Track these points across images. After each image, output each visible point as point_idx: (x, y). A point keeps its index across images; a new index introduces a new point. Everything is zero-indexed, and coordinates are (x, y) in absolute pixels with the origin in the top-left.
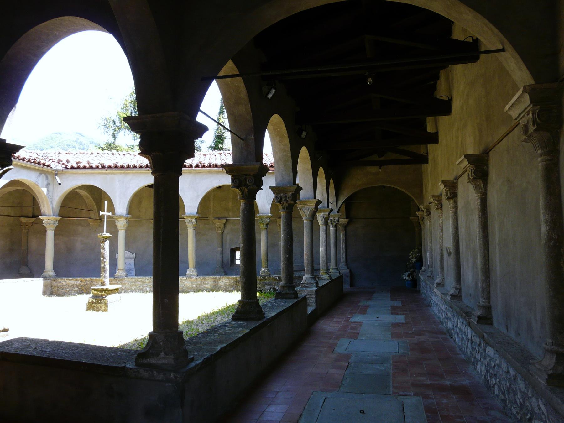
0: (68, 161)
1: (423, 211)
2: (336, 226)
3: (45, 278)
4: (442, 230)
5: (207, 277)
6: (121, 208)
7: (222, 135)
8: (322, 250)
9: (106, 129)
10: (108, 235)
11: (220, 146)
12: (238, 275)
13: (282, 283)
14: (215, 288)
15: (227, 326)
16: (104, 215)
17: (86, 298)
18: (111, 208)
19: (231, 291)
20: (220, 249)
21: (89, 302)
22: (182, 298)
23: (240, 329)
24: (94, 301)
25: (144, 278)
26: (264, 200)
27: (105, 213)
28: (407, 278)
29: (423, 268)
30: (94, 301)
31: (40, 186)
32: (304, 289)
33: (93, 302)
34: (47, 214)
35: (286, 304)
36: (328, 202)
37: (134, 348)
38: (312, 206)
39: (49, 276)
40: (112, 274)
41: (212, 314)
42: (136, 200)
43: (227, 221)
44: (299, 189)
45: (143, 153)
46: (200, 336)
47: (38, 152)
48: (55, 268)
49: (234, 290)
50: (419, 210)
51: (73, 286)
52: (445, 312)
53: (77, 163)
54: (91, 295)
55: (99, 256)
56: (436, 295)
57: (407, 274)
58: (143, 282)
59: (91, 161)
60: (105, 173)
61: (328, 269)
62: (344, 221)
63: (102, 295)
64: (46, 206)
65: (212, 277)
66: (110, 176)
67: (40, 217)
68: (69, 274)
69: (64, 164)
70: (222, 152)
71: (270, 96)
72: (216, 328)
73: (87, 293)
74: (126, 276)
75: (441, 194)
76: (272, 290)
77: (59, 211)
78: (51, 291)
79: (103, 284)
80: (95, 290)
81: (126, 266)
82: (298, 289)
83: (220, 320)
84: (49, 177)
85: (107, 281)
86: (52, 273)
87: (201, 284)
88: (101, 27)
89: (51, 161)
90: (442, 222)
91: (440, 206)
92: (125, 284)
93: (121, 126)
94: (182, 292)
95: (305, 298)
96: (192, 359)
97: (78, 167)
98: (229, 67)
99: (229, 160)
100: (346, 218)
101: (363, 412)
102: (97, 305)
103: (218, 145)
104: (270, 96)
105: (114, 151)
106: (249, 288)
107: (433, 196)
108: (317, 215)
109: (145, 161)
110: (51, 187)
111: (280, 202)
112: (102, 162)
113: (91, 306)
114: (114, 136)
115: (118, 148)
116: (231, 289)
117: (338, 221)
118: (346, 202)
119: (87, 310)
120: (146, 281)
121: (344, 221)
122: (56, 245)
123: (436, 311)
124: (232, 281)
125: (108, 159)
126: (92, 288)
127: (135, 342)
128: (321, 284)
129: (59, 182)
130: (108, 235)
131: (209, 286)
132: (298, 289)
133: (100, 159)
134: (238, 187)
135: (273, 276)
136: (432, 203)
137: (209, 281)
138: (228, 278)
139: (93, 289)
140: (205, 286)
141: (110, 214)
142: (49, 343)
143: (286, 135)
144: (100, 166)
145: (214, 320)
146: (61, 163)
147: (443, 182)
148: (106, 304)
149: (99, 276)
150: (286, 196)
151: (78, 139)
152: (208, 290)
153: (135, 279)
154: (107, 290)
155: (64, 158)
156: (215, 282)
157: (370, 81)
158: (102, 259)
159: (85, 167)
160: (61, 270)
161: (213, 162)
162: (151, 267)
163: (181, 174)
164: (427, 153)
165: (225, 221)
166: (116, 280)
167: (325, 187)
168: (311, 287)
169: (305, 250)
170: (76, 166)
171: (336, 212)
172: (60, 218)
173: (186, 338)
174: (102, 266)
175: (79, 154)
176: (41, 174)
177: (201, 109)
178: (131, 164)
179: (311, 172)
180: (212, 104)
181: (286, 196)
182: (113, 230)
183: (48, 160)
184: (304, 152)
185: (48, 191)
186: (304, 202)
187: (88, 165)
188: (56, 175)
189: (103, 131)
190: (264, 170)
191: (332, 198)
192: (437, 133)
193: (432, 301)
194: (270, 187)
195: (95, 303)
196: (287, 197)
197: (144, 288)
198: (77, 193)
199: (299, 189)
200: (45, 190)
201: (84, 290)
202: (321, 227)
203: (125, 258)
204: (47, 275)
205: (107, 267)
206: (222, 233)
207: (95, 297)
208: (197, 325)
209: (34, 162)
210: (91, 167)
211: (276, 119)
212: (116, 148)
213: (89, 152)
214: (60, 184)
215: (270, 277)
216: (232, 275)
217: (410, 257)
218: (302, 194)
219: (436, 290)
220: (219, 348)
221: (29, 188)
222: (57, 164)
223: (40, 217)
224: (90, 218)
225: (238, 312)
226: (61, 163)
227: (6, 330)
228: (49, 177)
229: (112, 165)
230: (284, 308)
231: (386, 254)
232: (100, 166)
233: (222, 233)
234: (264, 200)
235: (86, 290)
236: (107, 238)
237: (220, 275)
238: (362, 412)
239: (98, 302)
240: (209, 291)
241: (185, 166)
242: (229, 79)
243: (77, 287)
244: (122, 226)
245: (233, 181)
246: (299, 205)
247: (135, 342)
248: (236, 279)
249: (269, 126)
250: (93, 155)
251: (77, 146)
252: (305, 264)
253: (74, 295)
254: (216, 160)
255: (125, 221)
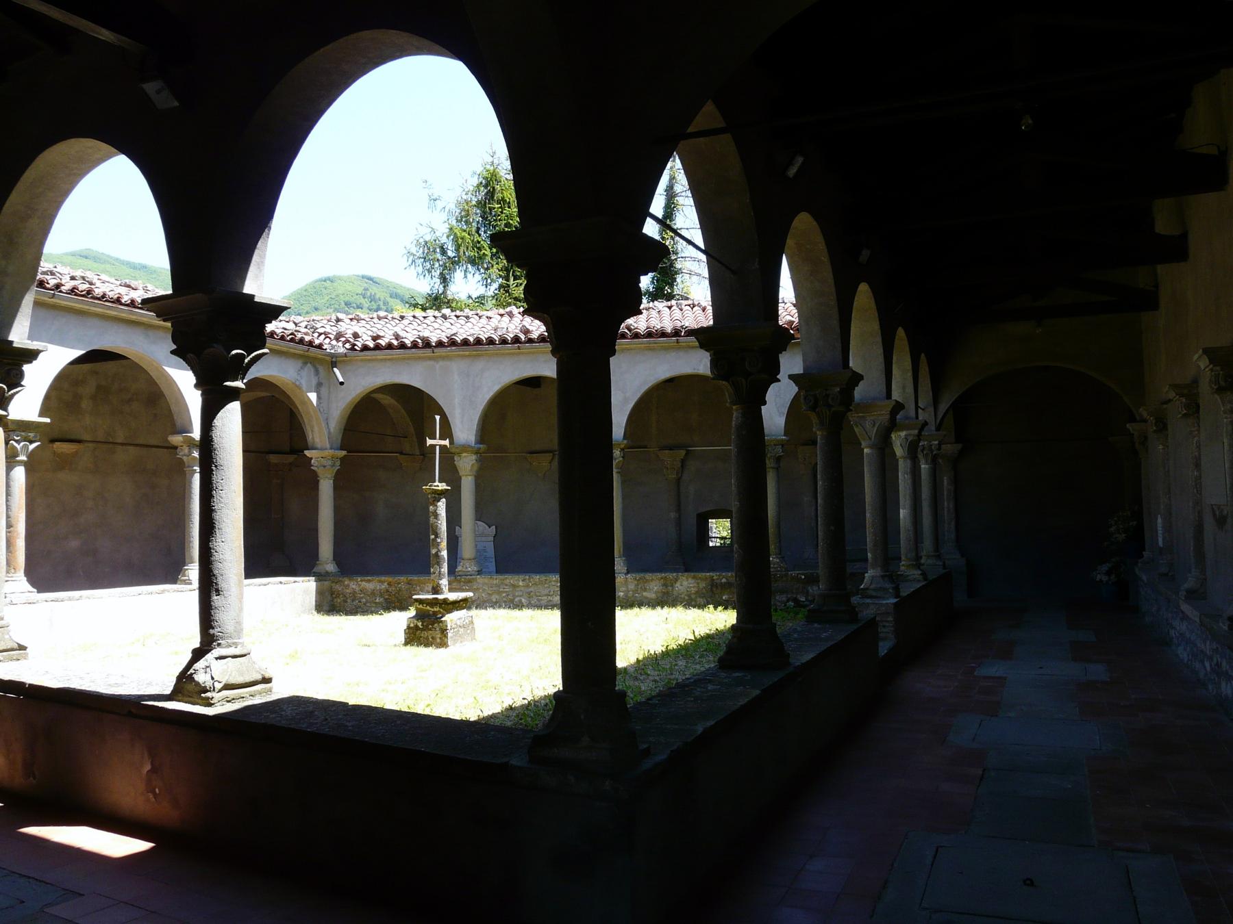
0: (356, 336)
1: (1145, 421)
2: (934, 461)
3: (320, 577)
4: (1198, 465)
5: (648, 576)
6: (465, 430)
8: (903, 513)
9: (428, 265)
10: (442, 486)
11: (667, 290)
14: (665, 600)
15: (710, 681)
16: (434, 446)
17: (400, 620)
18: (447, 432)
19: (701, 607)
20: (673, 515)
21: (409, 627)
22: (623, 618)
23: (740, 689)
24: (420, 624)
25: (516, 577)
28: (1105, 578)
29: (1146, 554)
30: (420, 624)
32: (868, 601)
34: (319, 446)
35: (831, 635)
36: (917, 407)
37: (509, 724)
38: (882, 416)
40: (452, 571)
41: (666, 654)
43: (688, 452)
44: (857, 378)
45: (532, 311)
46: (655, 701)
48: (338, 557)
49: (709, 603)
50: (1133, 419)
51: (373, 593)
52: (1211, 658)
53: (375, 338)
54: (412, 612)
55: (426, 530)
56: (1185, 617)
57: (1105, 568)
58: (514, 586)
59: (402, 334)
60: (430, 358)
61: (918, 558)
62: (951, 448)
63: (435, 613)
64: (316, 429)
65: (659, 575)
66: (441, 363)
67: (306, 452)
68: (364, 570)
70: (673, 302)
71: (792, 172)
72: (687, 686)
73: (403, 608)
74: (480, 572)
75: (1195, 382)
76: (791, 603)
78: (329, 604)
79: (436, 590)
80: (420, 601)
81: (478, 551)
83: (685, 671)
84: (321, 369)
85: (444, 582)
86: (331, 567)
87: (635, 591)
90: (1199, 447)
91: (1193, 409)
93: (459, 257)
94: (629, 604)
95: (872, 623)
96: (647, 753)
99: (707, 320)
100: (957, 442)
101: (1032, 884)
104: (792, 172)
105: (446, 311)
106: (752, 600)
107: (1174, 387)
108: (893, 436)
109: (537, 328)
110: (324, 390)
111: (813, 408)
112: (426, 334)
113: (414, 636)
114: (444, 280)
115: (454, 305)
116: (701, 601)
117: (939, 449)
118: (954, 406)
119: (406, 644)
121: (951, 448)
122: (337, 509)
123: (1183, 653)
124: (702, 585)
125: (436, 328)
127: (511, 713)
128: (906, 591)
129: (341, 380)
130: (442, 486)
131: (653, 596)
132: (855, 600)
133: (419, 328)
134: (726, 379)
135: (794, 573)
136: (1170, 401)
138: (694, 578)
139: (416, 600)
141: (446, 442)
143: (825, 259)
144: (420, 345)
147: (1206, 351)
148: (444, 631)
149: (429, 573)
150: (827, 396)
151: (366, 289)
152: (654, 604)
153: (497, 579)
154: (445, 601)
155: (348, 328)
156: (665, 585)
157: (1026, 123)
159: (390, 346)
160: (353, 561)
162: (555, 553)
163: (613, 352)
164: (1157, 286)
165: (683, 452)
166: (459, 581)
167: (910, 374)
168: (884, 598)
169: (868, 515)
170: (371, 344)
171: (933, 428)
172: (344, 453)
173: (630, 704)
174: (434, 551)
175: (376, 320)
176: (305, 363)
178: (483, 337)
179: (879, 339)
181: (827, 396)
184: (864, 295)
185: (319, 398)
186: (866, 407)
187: (395, 343)
188: (334, 364)
189: (420, 269)
190: (783, 338)
191: (925, 399)
192: (1184, 236)
193: (1172, 632)
195: (422, 630)
196: (826, 395)
198: (375, 401)
199: (857, 378)
200: (313, 396)
201: (394, 603)
202: (901, 463)
203: (476, 536)
205: (444, 553)
206: (678, 480)
207: (420, 616)
208: (636, 679)
209: (292, 340)
210: (402, 346)
211: (803, 222)
212: (448, 303)
213: (396, 315)
214: (342, 383)
215: (786, 575)
216: (702, 570)
217: (1112, 529)
218: (859, 392)
219: (1185, 607)
220: (700, 729)
222: (334, 342)
223: (306, 452)
224: (401, 453)
225: (730, 649)
227: (266, 680)
228: (321, 369)
229: (445, 340)
231: (1057, 519)
232: (420, 345)
233: (678, 480)
235: (400, 601)
236: (442, 493)
238: (1029, 882)
239: (427, 630)
240: (654, 607)
241: (624, 336)
242: (702, 139)
243: (381, 596)
244: (469, 468)
245: (714, 364)
246: (852, 417)
247: (511, 713)
249: (790, 242)
250: (405, 322)
252: (869, 545)
253: (376, 613)
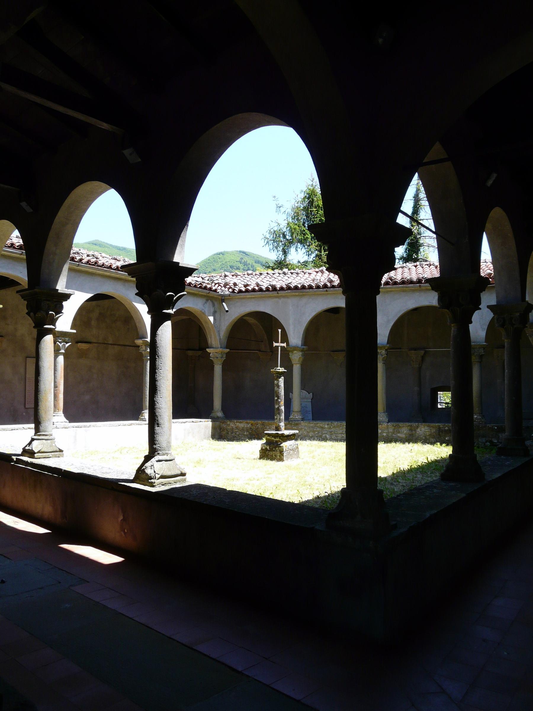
0: (235, 284)
3: (214, 420)
5: (401, 424)
6: (296, 338)
7: (417, 241)
9: (276, 244)
10: (282, 370)
12: (448, 422)
13: (503, 436)
14: (411, 439)
17: (257, 445)
18: (285, 338)
19: (433, 443)
20: (416, 389)
21: (262, 449)
22: (382, 447)
24: (268, 447)
25: (324, 423)
26: (479, 326)
27: (279, 344)
30: (268, 447)
31: (207, 314)
33: (266, 448)
34: (214, 346)
39: (218, 417)
40: (287, 418)
42: (316, 327)
43: (426, 352)
47: (204, 276)
48: (224, 409)
51: (243, 429)
53: (246, 286)
54: (264, 441)
55: (273, 394)
58: (322, 428)
59: (261, 283)
65: (408, 424)
66: (282, 299)
67: (207, 350)
69: (231, 288)
70: (418, 263)
71: (490, 183)
74: (303, 419)
76: (488, 444)
77: (227, 343)
78: (220, 434)
79: (278, 428)
80: (269, 435)
81: (302, 407)
82: (528, 443)
85: (282, 424)
86: (220, 414)
87: (393, 433)
88: (279, 120)
89: (217, 285)
92: (302, 429)
93: (293, 239)
97: (247, 291)
98: (437, 151)
99: (434, 272)
102: (271, 453)
103: (412, 256)
104: (490, 183)
105: (286, 270)
110: (217, 315)
111: (503, 326)
112: (274, 283)
113: (265, 454)
114: (285, 253)
116: (432, 440)
119: (260, 458)
120: (326, 426)
122: (224, 382)
124: (433, 430)
125: (280, 280)
126: (266, 432)
127: (318, 500)
129: (227, 309)
130: (282, 370)
132: (528, 443)
133: (270, 280)
135: (490, 426)
137: (404, 430)
139: (266, 434)
140: (398, 435)
141: (284, 345)
142: (227, 493)
143: (511, 235)
145: (413, 479)
146: (228, 287)
148: (281, 452)
151: (242, 259)
152: (403, 441)
158: (276, 398)
159: (254, 290)
161: (407, 276)
163: (378, 293)
165: (422, 352)
172: (228, 350)
174: (276, 407)
175: (246, 276)
176: (207, 300)
177: (402, 209)
178: (306, 285)
180: (415, 204)
182: (287, 363)
183: (213, 284)
185: (215, 319)
187: (257, 288)
188: (223, 301)
189: (271, 246)
194: (488, 307)
195: (269, 451)
197: (324, 435)
200: (211, 319)
201: (255, 435)
204: (216, 416)
205: (283, 408)
206: (420, 368)
207: (268, 443)
208: (392, 484)
210: (261, 290)
211: (497, 213)
212: (287, 266)
213: (258, 273)
214: (227, 311)
220: (428, 515)
221: (195, 317)
222: (223, 288)
223: (207, 350)
224: (260, 351)
226: (228, 287)
228: (216, 303)
230: (511, 468)
233: (420, 368)
234: (479, 326)
235: (257, 434)
236: (282, 374)
237: (418, 421)
239: (272, 451)
243: (247, 431)
244: (297, 359)
245: (440, 300)
247: (318, 500)
248: (439, 428)
249: (488, 225)
251: (241, 266)
253: (245, 440)
254: (410, 274)
255: (301, 353)
